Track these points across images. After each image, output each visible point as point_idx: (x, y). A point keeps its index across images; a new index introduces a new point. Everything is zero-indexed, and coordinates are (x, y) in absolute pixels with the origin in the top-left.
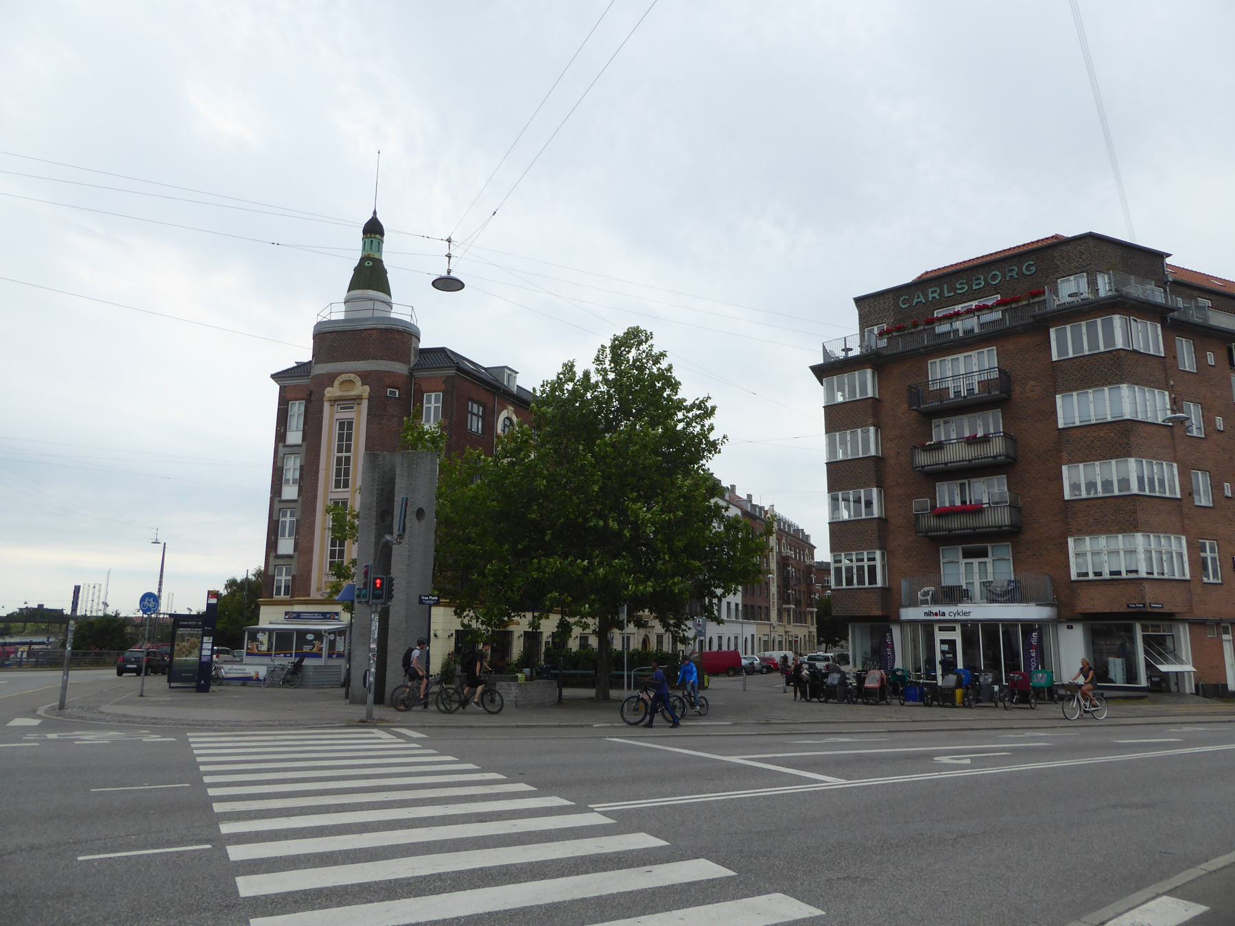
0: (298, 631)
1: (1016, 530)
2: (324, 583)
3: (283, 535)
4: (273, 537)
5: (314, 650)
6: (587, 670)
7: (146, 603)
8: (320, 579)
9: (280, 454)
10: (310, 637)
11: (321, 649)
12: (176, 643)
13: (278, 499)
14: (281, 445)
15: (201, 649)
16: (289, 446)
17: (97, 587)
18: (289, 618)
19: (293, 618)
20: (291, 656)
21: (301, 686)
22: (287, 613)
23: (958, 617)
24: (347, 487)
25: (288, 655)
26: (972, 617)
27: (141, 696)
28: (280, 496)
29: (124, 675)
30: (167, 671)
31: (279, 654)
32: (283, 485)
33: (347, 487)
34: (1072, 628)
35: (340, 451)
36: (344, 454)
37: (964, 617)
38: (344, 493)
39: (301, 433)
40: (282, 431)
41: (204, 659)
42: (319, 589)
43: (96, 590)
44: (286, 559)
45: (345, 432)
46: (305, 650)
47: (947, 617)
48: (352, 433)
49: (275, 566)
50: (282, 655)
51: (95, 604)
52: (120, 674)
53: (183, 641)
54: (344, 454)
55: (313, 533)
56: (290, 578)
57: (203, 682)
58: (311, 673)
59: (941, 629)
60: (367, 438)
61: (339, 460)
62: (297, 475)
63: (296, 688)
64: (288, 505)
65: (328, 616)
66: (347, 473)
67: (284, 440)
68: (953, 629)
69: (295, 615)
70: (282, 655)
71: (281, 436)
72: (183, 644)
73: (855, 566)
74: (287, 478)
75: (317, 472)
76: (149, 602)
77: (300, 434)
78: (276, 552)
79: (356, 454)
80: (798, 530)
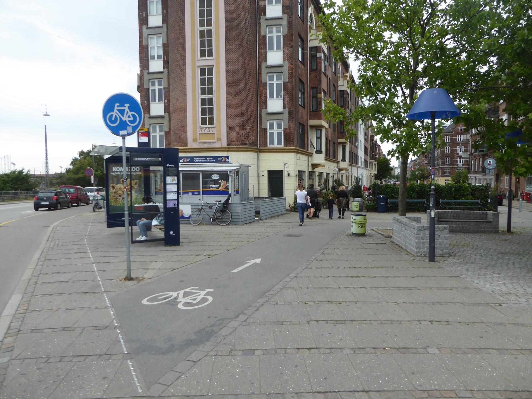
0: (203, 172)
2: (198, 135)
3: (154, 100)
4: (146, 102)
5: (220, 188)
6: (412, 199)
7: (115, 113)
8: (195, 132)
9: (145, 35)
10: (215, 177)
11: (227, 188)
12: (111, 185)
13: (147, 71)
14: (144, 27)
15: (165, 192)
16: (152, 28)
17: (6, 157)
18: (184, 162)
19: (188, 162)
20: (199, 194)
21: (231, 223)
24: (212, 56)
25: (197, 193)
27: (129, 278)
28: (148, 69)
29: (40, 209)
31: (187, 193)
32: (149, 60)
33: (212, 56)
35: (202, 25)
36: (206, 28)
38: (207, 61)
39: (161, 17)
40: (144, 15)
41: (170, 205)
42: (195, 140)
43: (6, 159)
44: (159, 119)
45: (205, 9)
46: (211, 189)
48: (211, 9)
49: (150, 124)
50: (190, 193)
51: (6, 166)
52: (36, 209)
53: (118, 183)
54: (206, 28)
55: (185, 95)
56: (163, 134)
57: (171, 233)
58: (239, 211)
60: (226, 13)
61: (202, 33)
62: (161, 52)
63: (228, 224)
64: (156, 76)
65: (219, 159)
66: (210, 44)
67: (147, 24)
69: (188, 160)
70: (190, 193)
71: (143, 20)
72: (118, 186)
74: (152, 54)
75: (184, 44)
76: (122, 112)
77: (160, 18)
78: (149, 114)
79: (218, 27)
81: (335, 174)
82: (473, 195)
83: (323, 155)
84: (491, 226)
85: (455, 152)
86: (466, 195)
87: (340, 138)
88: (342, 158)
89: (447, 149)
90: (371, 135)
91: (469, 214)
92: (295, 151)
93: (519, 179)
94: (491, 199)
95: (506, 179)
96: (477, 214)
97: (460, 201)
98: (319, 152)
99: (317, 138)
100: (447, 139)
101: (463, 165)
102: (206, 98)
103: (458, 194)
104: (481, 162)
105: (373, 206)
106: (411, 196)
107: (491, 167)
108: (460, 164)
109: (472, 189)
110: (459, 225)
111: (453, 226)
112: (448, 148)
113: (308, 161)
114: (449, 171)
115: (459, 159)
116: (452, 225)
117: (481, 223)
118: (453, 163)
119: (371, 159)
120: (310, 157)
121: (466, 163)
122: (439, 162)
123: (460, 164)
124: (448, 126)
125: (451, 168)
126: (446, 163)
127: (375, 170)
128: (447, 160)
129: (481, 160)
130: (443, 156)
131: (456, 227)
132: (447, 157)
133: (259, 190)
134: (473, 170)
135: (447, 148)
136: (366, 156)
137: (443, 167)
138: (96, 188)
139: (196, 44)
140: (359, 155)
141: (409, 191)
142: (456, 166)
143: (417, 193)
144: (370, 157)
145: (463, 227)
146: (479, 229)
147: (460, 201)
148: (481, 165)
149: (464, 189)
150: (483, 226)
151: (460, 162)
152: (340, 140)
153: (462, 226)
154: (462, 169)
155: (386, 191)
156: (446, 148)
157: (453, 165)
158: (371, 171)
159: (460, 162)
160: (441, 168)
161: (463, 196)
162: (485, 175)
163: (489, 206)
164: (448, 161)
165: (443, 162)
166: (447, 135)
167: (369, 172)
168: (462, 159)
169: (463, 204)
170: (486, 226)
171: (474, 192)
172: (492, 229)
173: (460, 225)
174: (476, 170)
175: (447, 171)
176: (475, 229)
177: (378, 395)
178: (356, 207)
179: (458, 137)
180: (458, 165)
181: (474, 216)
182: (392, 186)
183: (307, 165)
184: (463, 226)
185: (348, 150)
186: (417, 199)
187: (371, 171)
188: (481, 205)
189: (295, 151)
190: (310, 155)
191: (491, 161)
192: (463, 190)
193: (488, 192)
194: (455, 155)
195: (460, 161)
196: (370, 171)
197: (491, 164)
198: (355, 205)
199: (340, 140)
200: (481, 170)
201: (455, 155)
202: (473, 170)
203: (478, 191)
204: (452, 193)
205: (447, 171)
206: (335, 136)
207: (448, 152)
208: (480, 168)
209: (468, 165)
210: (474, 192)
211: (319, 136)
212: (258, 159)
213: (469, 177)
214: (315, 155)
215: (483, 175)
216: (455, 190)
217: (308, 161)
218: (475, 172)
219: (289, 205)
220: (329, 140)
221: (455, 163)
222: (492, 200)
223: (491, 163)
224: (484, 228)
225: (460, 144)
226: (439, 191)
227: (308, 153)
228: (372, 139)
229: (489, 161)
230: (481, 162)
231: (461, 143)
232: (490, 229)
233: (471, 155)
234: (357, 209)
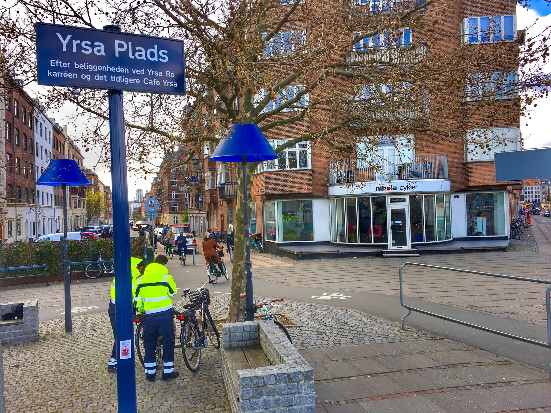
1: (315, 106)
22: (261, 234)
23: (407, 191)
24: (433, 239)
26: (418, 190)
30: (194, 244)
34: (458, 197)
37: (411, 191)
47: (398, 191)
59: (392, 201)
68: (403, 200)
73: (298, 152)
80: (47, 285)
89: (174, 181)
102: (412, 244)
126: (174, 197)
128: (175, 194)
132: (174, 190)
133: (271, 126)
137: (171, 203)
138: (37, 266)
139: (435, 220)
157: (181, 199)
158: (74, 210)
164: (176, 195)
177: (341, 381)
191: (153, 201)
224: (8, 335)
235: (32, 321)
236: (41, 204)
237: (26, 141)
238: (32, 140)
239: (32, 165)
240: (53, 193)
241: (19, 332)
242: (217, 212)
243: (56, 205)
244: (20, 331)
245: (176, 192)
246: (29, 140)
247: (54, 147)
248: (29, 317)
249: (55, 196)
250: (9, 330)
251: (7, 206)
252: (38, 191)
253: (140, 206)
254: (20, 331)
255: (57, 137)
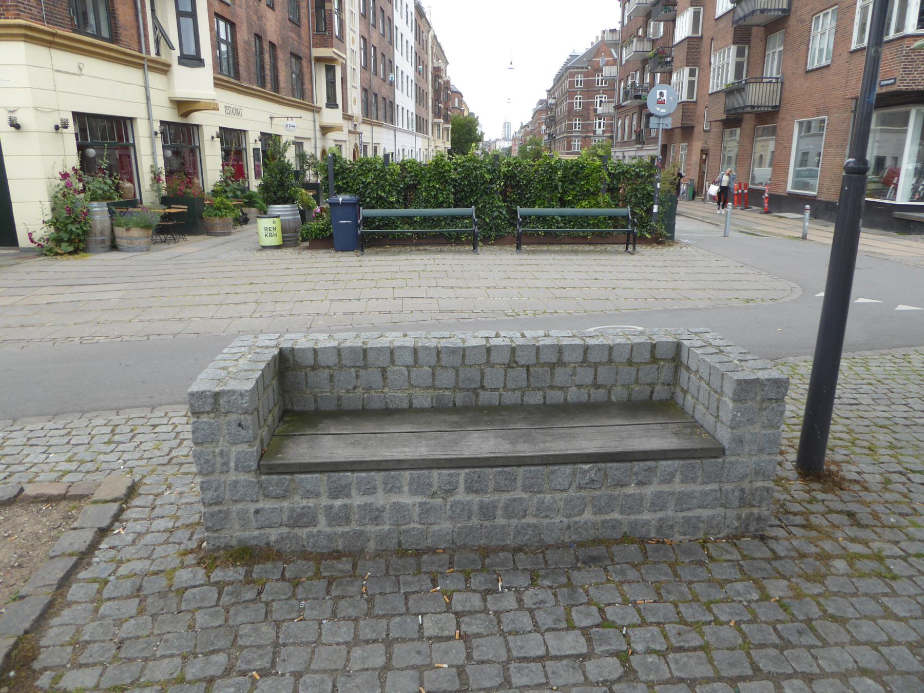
6: (440, 205)
81: (310, 139)
82: (612, 190)
83: (207, 73)
84: (714, 486)
85: (591, 108)
86: (593, 194)
87: (317, 45)
88: (328, 98)
89: (578, 101)
90: (436, 65)
91: (552, 366)
92: (26, 36)
93: (706, 154)
94: (661, 204)
95: (682, 155)
96: (610, 361)
97: (577, 210)
98: (192, 60)
99: (180, 14)
100: (577, 81)
101: (604, 132)
103: (574, 189)
104: (635, 123)
105: (322, 230)
106: (436, 197)
107: (663, 111)
108: (599, 131)
109: (610, 174)
110: (451, 491)
111: (398, 508)
112: (580, 98)
113: (314, 121)
114: (580, 143)
115: (598, 121)
116: (394, 498)
117: (638, 466)
118: (587, 128)
119: (437, 114)
120: (316, 115)
121: (609, 129)
122: (564, 125)
123: (599, 131)
124: (581, 55)
125: (583, 137)
126: (575, 128)
127: (448, 140)
128: (577, 122)
129: (635, 116)
130: (571, 113)
131: (425, 510)
134: (619, 140)
135: (578, 99)
136: (423, 110)
137: (570, 137)
140: (397, 102)
141: (429, 181)
142: (592, 135)
143: (454, 187)
144: (433, 112)
145: (487, 512)
146: (616, 515)
147: (577, 210)
148: (634, 128)
149: (590, 175)
150: (649, 491)
151: (600, 126)
152: (318, 52)
153: (475, 499)
154: (602, 141)
155: (363, 183)
156: (577, 99)
157: (587, 132)
158: (437, 141)
159: (600, 126)
160: (566, 137)
161: (589, 195)
162: (641, 149)
163: (653, 223)
164: (579, 124)
165: (570, 126)
166: (578, 73)
167: (432, 143)
168: (602, 121)
169: (582, 221)
170: (678, 486)
171: (615, 182)
172: (720, 511)
173: (461, 496)
174: (626, 139)
175: (576, 143)
176: (588, 515)
178: (271, 235)
179: (597, 78)
180: (594, 132)
181: (586, 375)
182: (379, 167)
183: (144, 100)
184: (487, 498)
185: (358, 85)
186: (455, 206)
187: (437, 141)
188: (634, 224)
189: (26, 36)
190: (164, 69)
191: (665, 92)
192: (587, 177)
193: (653, 184)
194: (591, 112)
195: (600, 123)
196: (434, 140)
197: (663, 102)
198: (266, 229)
199: (318, 52)
200: (634, 138)
201: (591, 112)
202: (619, 140)
203: (628, 179)
204: (556, 187)
205: (576, 143)
206: (299, 36)
207: (580, 106)
208: (633, 133)
209: (612, 132)
210: (615, 182)
211: (189, 10)
212: (148, 104)
213: (613, 154)
214: (180, 72)
215: (638, 149)
216: (564, 179)
217: (314, 121)
218: (624, 143)
219: (30, 234)
220: (272, 45)
221: (590, 129)
222: (663, 208)
223: (665, 97)
224: (658, 503)
225: (599, 91)
226: (519, 182)
227: (313, 107)
228: (437, 73)
229: (658, 92)
230: (635, 123)
231: (603, 90)
232: (705, 513)
233: (618, 107)
234: (276, 240)
235: (761, 450)
236: (400, 126)
237: (383, 21)
238: (391, 21)
239: (390, 62)
240: (414, 112)
241: (705, 494)
242: (689, 148)
243: (417, 131)
244: (709, 487)
245: (579, 120)
246: (386, 19)
247: (416, 39)
248: (757, 428)
249: (416, 116)
250: (663, 482)
251: (363, 122)
252: (398, 106)
253: (510, 145)
254: (709, 487)
255: (419, 22)
